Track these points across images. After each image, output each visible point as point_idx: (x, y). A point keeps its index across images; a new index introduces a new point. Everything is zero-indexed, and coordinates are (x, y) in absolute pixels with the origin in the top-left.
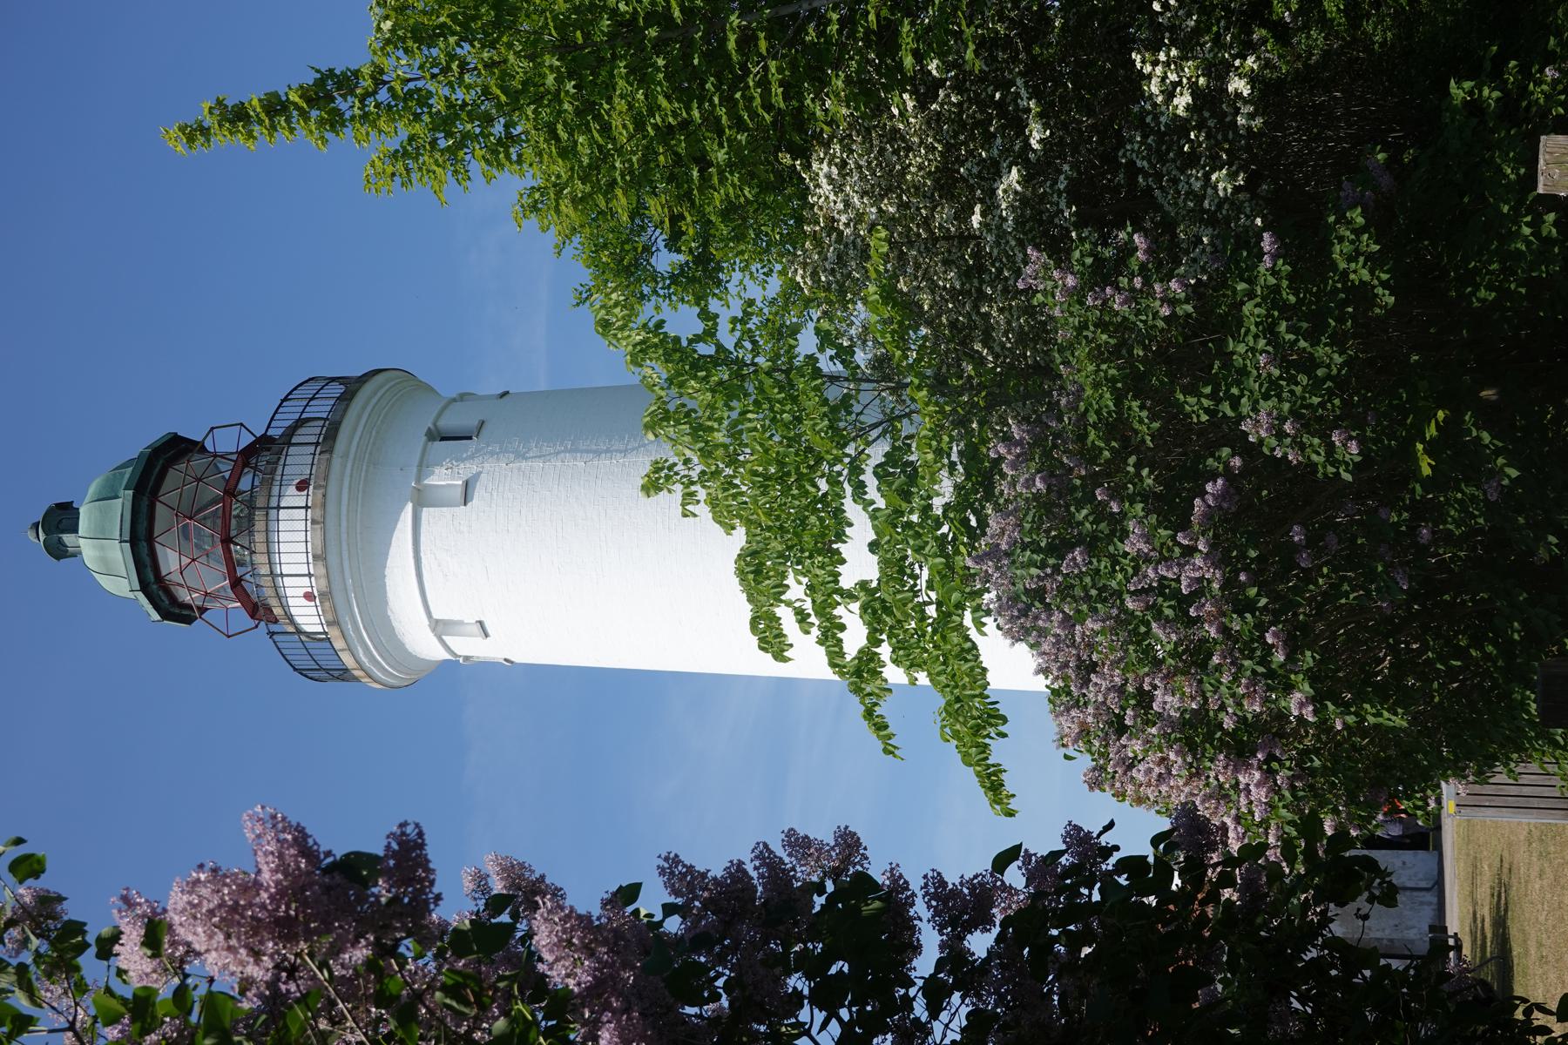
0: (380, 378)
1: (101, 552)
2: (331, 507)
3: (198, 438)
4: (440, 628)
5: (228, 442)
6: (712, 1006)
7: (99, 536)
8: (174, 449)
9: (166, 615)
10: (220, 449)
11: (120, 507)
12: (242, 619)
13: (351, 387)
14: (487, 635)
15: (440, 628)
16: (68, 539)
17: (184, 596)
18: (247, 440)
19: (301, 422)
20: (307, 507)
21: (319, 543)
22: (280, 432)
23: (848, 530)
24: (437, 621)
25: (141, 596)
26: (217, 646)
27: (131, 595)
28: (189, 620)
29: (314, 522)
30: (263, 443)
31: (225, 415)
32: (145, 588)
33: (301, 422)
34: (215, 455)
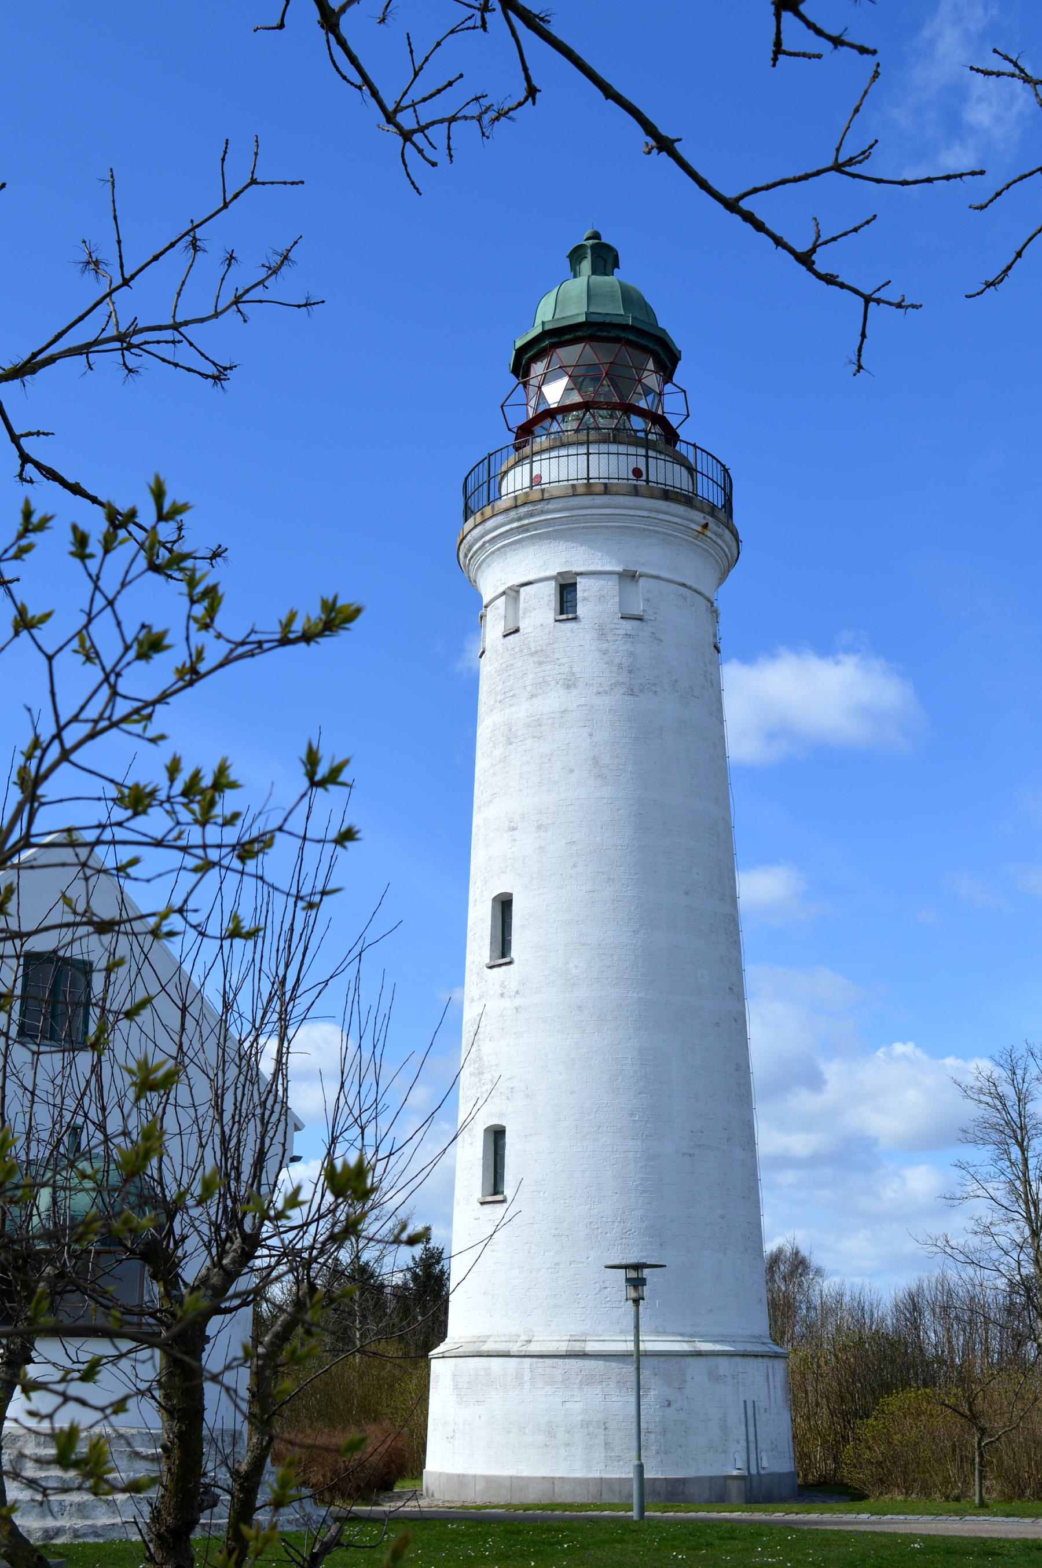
0: (734, 543)
1: (566, 299)
2: (587, 500)
3: (675, 379)
4: (513, 594)
5: (672, 407)
6: (413, 1503)
7: (591, 295)
8: (667, 359)
9: (520, 352)
10: (666, 399)
11: (614, 309)
12: (518, 419)
13: (723, 512)
14: (505, 636)
15: (513, 593)
16: (586, 266)
17: (538, 369)
18: (674, 421)
19: (691, 470)
20: (588, 478)
21: (556, 493)
22: (684, 452)
23: (73, 549)
24: (518, 592)
25: (537, 330)
26: (489, 401)
27: (538, 322)
28: (515, 371)
29: (573, 486)
30: (671, 436)
31: (699, 400)
32: (545, 334)
33: (691, 470)
34: (660, 394)
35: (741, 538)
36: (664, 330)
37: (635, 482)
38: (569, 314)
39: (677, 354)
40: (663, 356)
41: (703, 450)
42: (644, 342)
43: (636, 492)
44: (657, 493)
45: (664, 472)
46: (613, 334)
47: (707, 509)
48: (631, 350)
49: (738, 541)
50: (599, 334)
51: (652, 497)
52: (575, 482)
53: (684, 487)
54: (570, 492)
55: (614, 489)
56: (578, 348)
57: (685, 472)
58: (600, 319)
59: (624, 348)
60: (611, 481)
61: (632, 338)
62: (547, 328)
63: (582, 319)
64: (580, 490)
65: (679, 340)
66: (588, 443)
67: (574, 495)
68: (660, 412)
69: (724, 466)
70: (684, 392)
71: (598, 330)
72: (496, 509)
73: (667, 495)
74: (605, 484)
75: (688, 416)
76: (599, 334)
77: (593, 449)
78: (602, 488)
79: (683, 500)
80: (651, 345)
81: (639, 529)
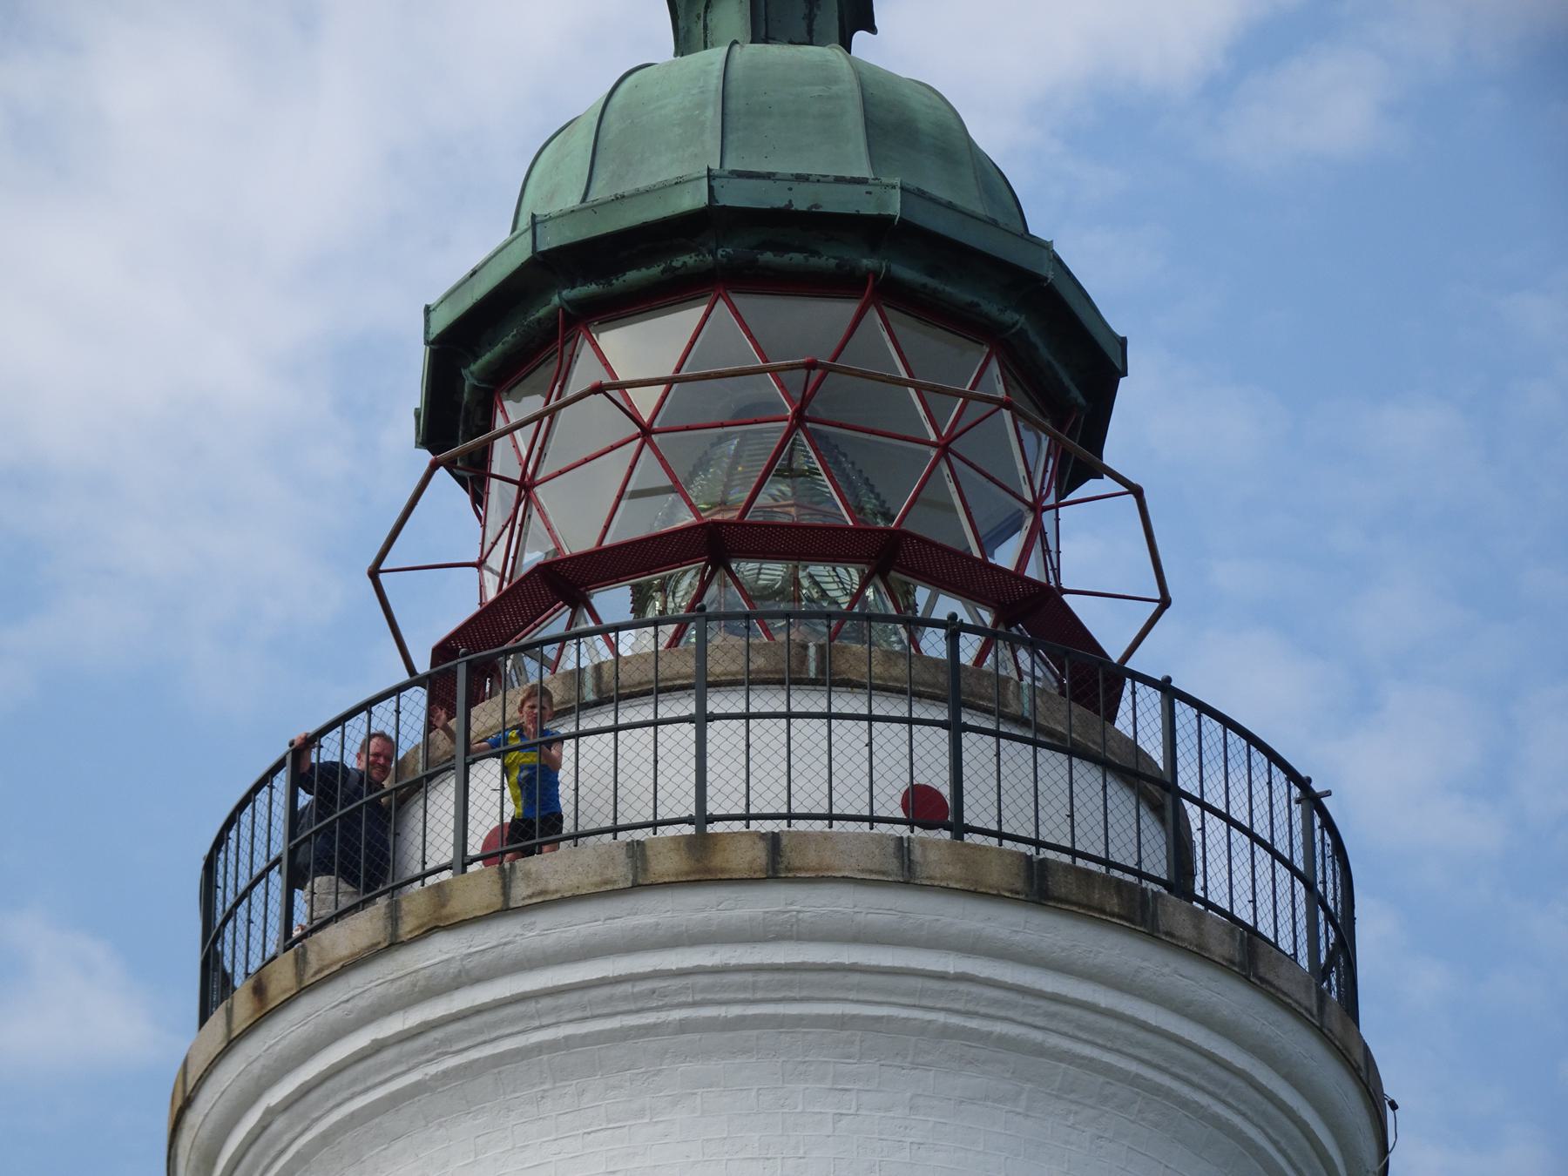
3: (1112, 455)
5: (1090, 551)
7: (733, 109)
8: (1061, 367)
11: (830, 164)
18: (1110, 628)
20: (702, 818)
35: (1390, 1090)
36: (1045, 246)
37: (902, 831)
38: (642, 184)
39: (1112, 352)
40: (1044, 353)
41: (1202, 708)
42: (959, 293)
43: (905, 872)
44: (995, 875)
45: (1021, 790)
46: (826, 261)
47: (1222, 947)
48: (906, 326)
49: (1377, 1104)
50: (768, 257)
51: (976, 892)
52: (639, 835)
53: (1123, 853)
54: (621, 873)
55: (812, 857)
56: (687, 319)
57: (1122, 801)
58: (772, 197)
59: (873, 315)
60: (800, 826)
61: (907, 273)
62: (551, 240)
63: (693, 199)
64: (665, 864)
65: (1106, 267)
66: (702, 685)
67: (637, 887)
68: (1033, 571)
69: (1304, 784)
70: (1137, 492)
71: (764, 246)
72: (314, 962)
73: (1041, 882)
74: (774, 840)
75: (1165, 602)
76: (768, 257)
77: (716, 703)
78: (760, 854)
79: (1113, 904)
80: (991, 308)
81: (922, 1029)
